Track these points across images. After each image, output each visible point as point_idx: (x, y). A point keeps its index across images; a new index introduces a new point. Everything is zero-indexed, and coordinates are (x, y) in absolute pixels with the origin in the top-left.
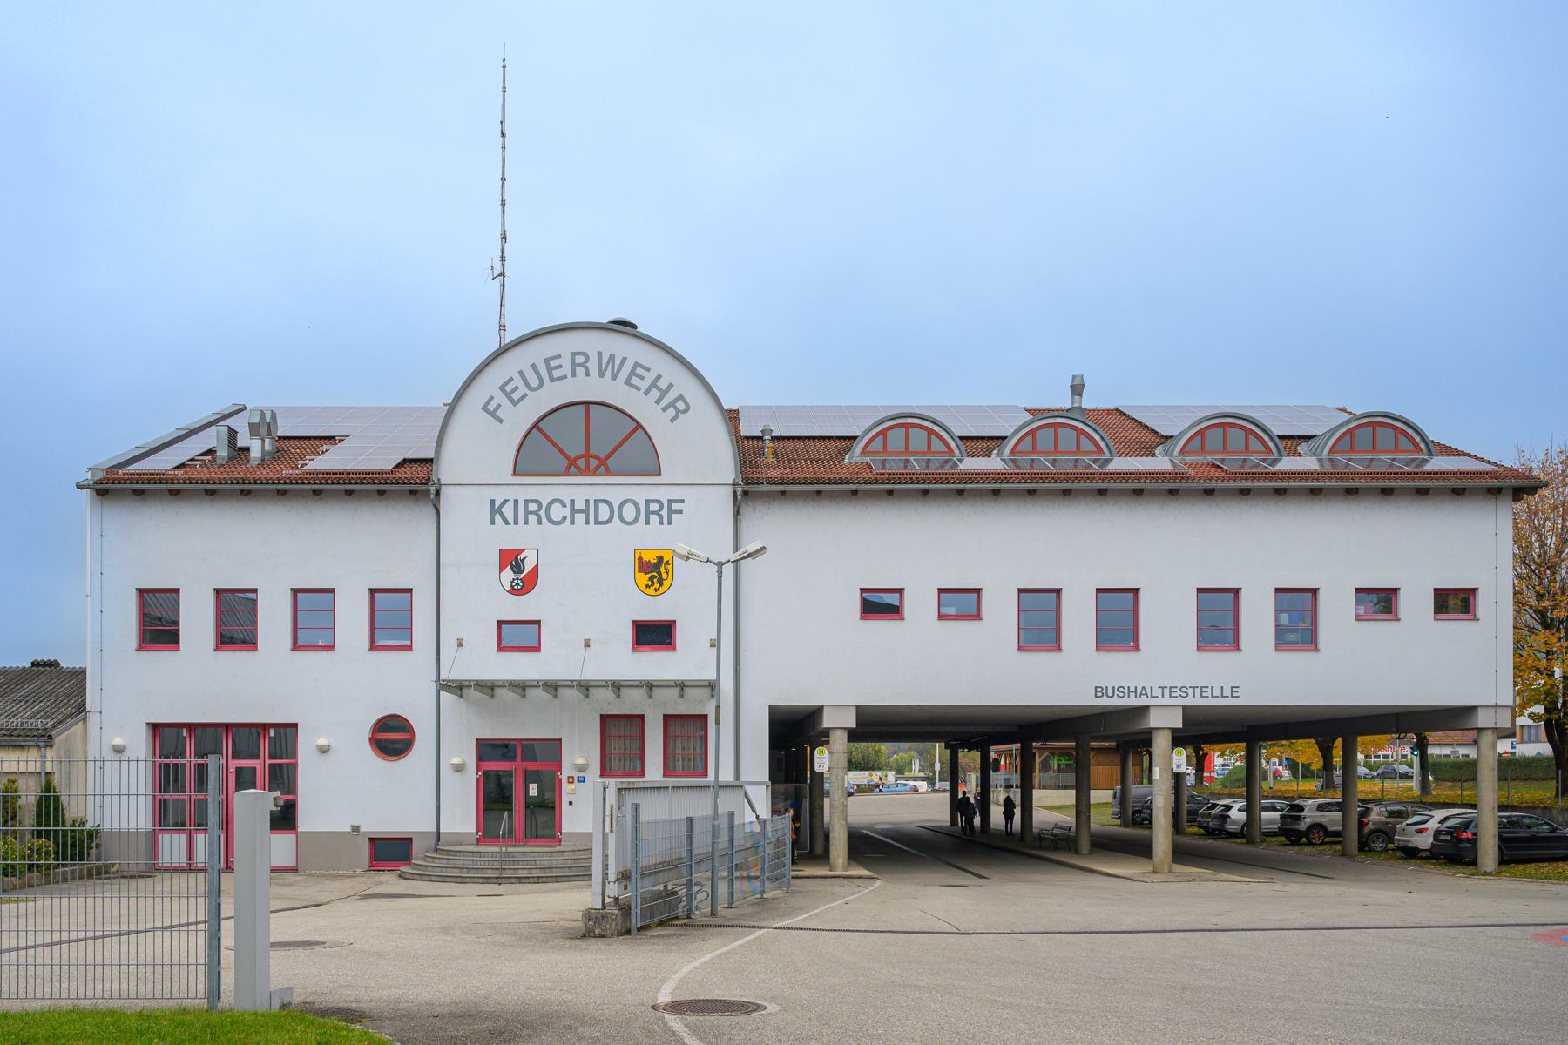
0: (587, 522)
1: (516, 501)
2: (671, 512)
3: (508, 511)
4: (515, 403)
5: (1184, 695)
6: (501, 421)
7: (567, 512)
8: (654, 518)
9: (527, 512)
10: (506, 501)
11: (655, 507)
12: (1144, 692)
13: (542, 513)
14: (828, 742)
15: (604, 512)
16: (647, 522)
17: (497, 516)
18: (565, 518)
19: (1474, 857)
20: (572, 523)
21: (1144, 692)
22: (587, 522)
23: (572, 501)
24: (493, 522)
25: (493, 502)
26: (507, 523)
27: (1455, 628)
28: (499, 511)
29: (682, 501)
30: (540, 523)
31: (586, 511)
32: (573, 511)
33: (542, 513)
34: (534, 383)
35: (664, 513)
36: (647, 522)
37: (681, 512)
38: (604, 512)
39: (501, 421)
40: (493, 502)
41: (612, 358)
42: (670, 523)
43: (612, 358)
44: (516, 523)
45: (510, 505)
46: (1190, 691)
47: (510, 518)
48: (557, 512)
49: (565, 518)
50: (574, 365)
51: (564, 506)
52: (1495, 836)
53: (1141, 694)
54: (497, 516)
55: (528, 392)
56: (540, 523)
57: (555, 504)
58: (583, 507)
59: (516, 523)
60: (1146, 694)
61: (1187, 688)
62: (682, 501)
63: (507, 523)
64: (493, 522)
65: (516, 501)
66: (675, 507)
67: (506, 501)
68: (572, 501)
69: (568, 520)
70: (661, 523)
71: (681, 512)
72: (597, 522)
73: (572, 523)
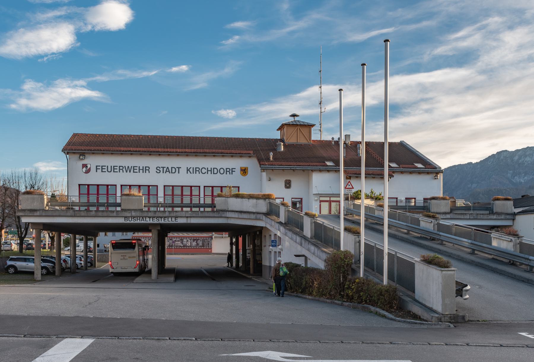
0: (211, 173)
1: (193, 168)
2: (232, 171)
3: (191, 170)
4: (102, 171)
5: (158, 168)
6: (97, 171)
7: (206, 171)
8: (228, 173)
9: (196, 171)
10: (191, 168)
11: (228, 170)
12: (168, 170)
13: (200, 171)
14: (279, 295)
15: (216, 171)
16: (226, 174)
17: (188, 172)
18: (205, 172)
19: (461, 284)
20: (208, 173)
21: (168, 170)
22: (211, 173)
23: (208, 168)
24: (187, 173)
25: (187, 168)
26: (191, 173)
27: (293, 184)
28: (189, 170)
29: (235, 169)
30: (199, 173)
31: (211, 171)
32: (208, 171)
33: (200, 171)
34: (109, 170)
35: (231, 171)
36: (226, 174)
37: (235, 171)
38: (216, 171)
39: (97, 171)
40: (187, 168)
41: (128, 167)
42: (232, 174)
43: (128, 167)
44: (193, 173)
45: (192, 169)
46: (161, 169)
47: (192, 172)
48: (204, 171)
49: (205, 172)
50: (120, 169)
51: (205, 169)
52: (348, 233)
53: (166, 171)
54: (188, 172)
55: (107, 171)
56: (199, 173)
57: (203, 169)
58: (210, 170)
59: (193, 173)
60: (169, 171)
61: (160, 168)
62: (235, 169)
63: (191, 173)
64: (187, 173)
65: (193, 168)
66: (233, 170)
67: (191, 168)
68: (208, 168)
69: (207, 173)
70: (230, 174)
71: (235, 171)
72: (214, 173)
73: (208, 173)
